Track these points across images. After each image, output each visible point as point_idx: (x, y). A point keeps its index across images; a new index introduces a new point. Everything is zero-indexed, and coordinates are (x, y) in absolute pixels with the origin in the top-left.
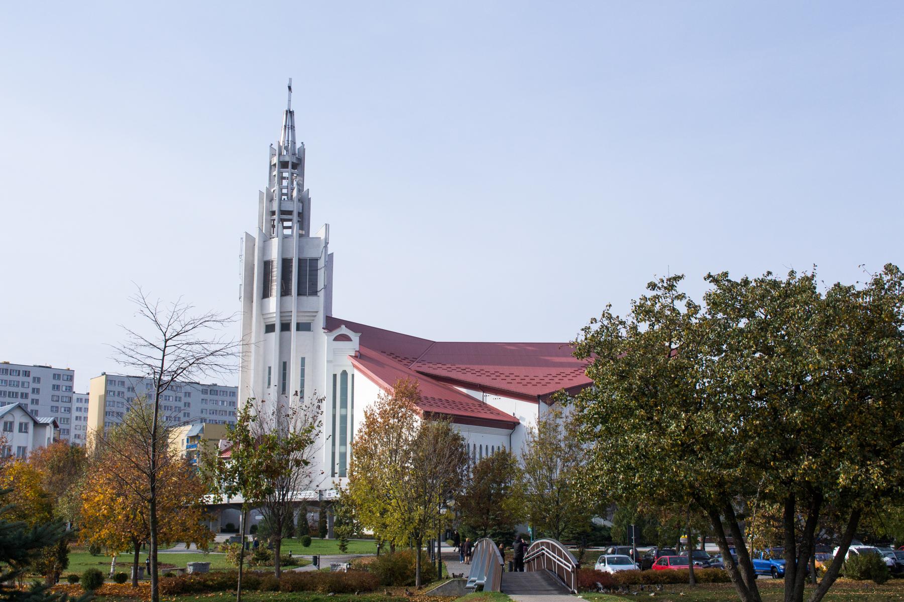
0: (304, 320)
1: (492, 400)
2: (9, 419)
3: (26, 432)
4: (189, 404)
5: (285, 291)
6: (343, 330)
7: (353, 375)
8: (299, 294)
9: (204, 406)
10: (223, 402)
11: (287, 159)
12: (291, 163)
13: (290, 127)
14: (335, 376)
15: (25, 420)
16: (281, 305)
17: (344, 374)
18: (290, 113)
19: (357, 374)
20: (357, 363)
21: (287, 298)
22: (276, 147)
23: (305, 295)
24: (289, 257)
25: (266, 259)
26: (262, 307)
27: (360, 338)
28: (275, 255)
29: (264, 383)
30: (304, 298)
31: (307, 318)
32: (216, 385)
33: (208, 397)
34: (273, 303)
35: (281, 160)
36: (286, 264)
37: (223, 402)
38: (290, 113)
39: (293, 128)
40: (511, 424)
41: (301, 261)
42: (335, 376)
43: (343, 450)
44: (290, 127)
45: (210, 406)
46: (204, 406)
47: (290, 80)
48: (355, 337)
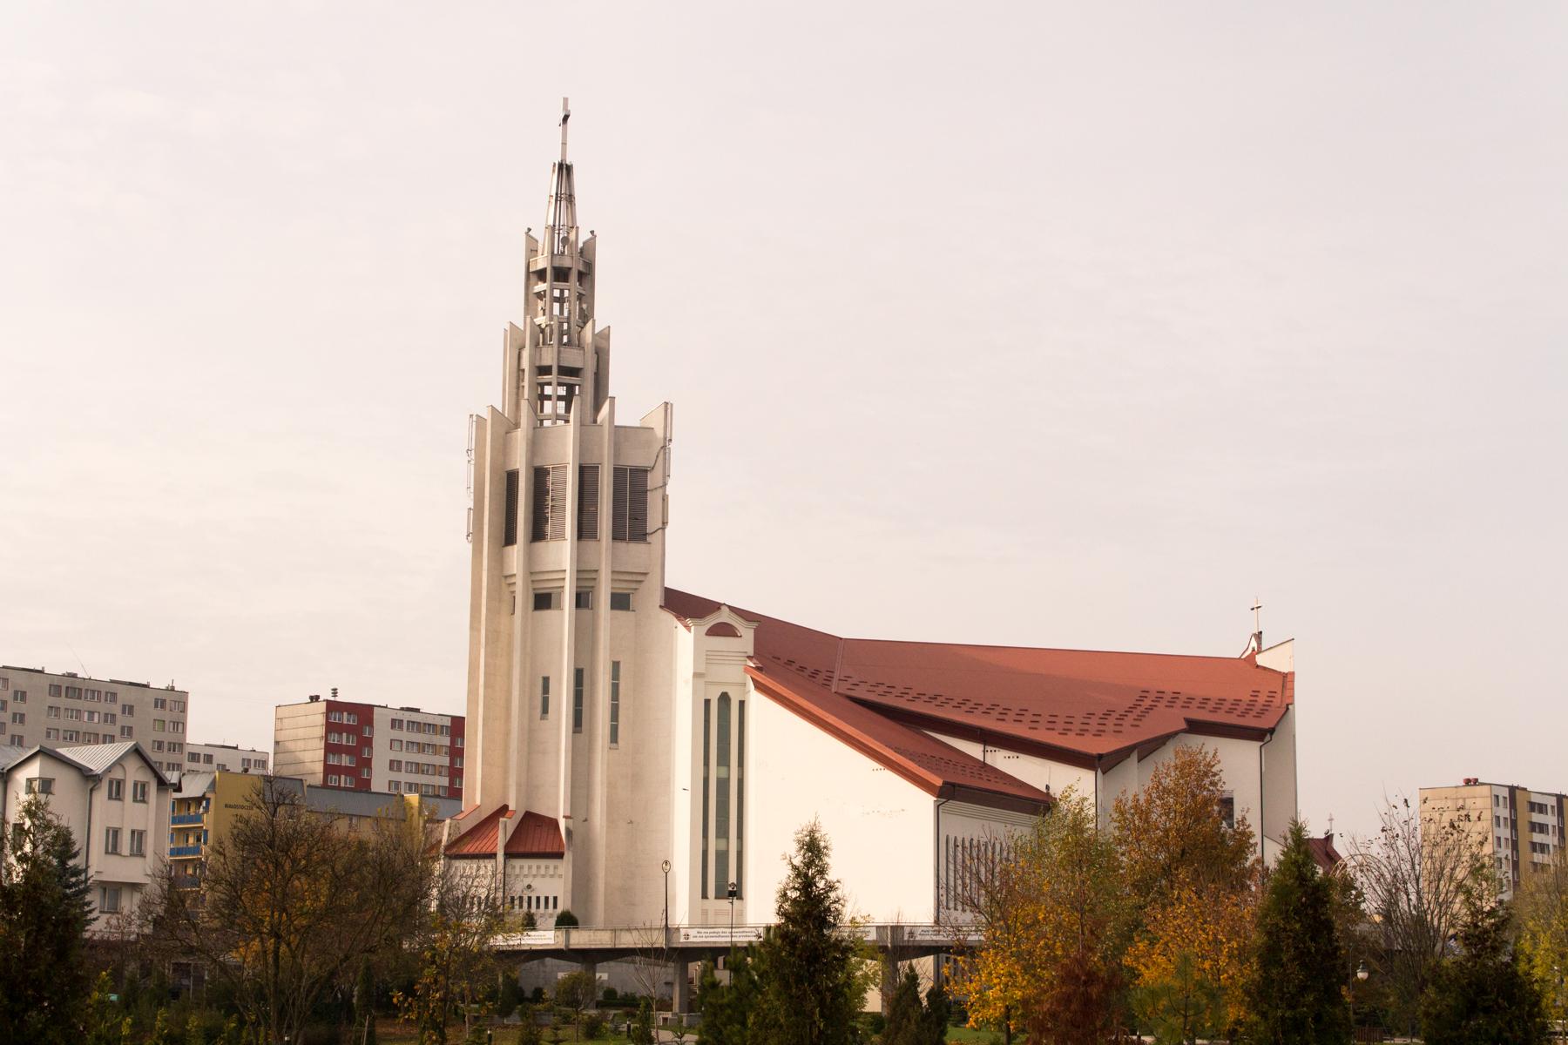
0: (622, 588)
1: (1002, 760)
2: (117, 774)
3: (143, 801)
4: (22, 716)
5: (585, 530)
6: (725, 617)
7: (742, 703)
8: (617, 536)
9: (54, 722)
10: (91, 713)
11: (567, 263)
12: (568, 273)
13: (566, 198)
14: (707, 702)
15: (144, 776)
16: (579, 557)
17: (725, 699)
18: (565, 170)
19: (758, 704)
20: (762, 678)
21: (591, 544)
22: (541, 235)
23: (623, 539)
24: (589, 461)
25: (538, 464)
26: (499, 561)
27: (756, 632)
28: (564, 451)
29: (532, 708)
30: (622, 545)
31: (624, 585)
32: (74, 676)
33: (63, 702)
34: (516, 555)
35: (557, 264)
36: (587, 475)
37: (91, 713)
38: (565, 170)
39: (570, 198)
40: (1039, 804)
41: (619, 472)
42: (707, 702)
43: (723, 847)
44: (566, 198)
45: (64, 723)
46: (54, 722)
47: (566, 100)
48: (747, 634)
